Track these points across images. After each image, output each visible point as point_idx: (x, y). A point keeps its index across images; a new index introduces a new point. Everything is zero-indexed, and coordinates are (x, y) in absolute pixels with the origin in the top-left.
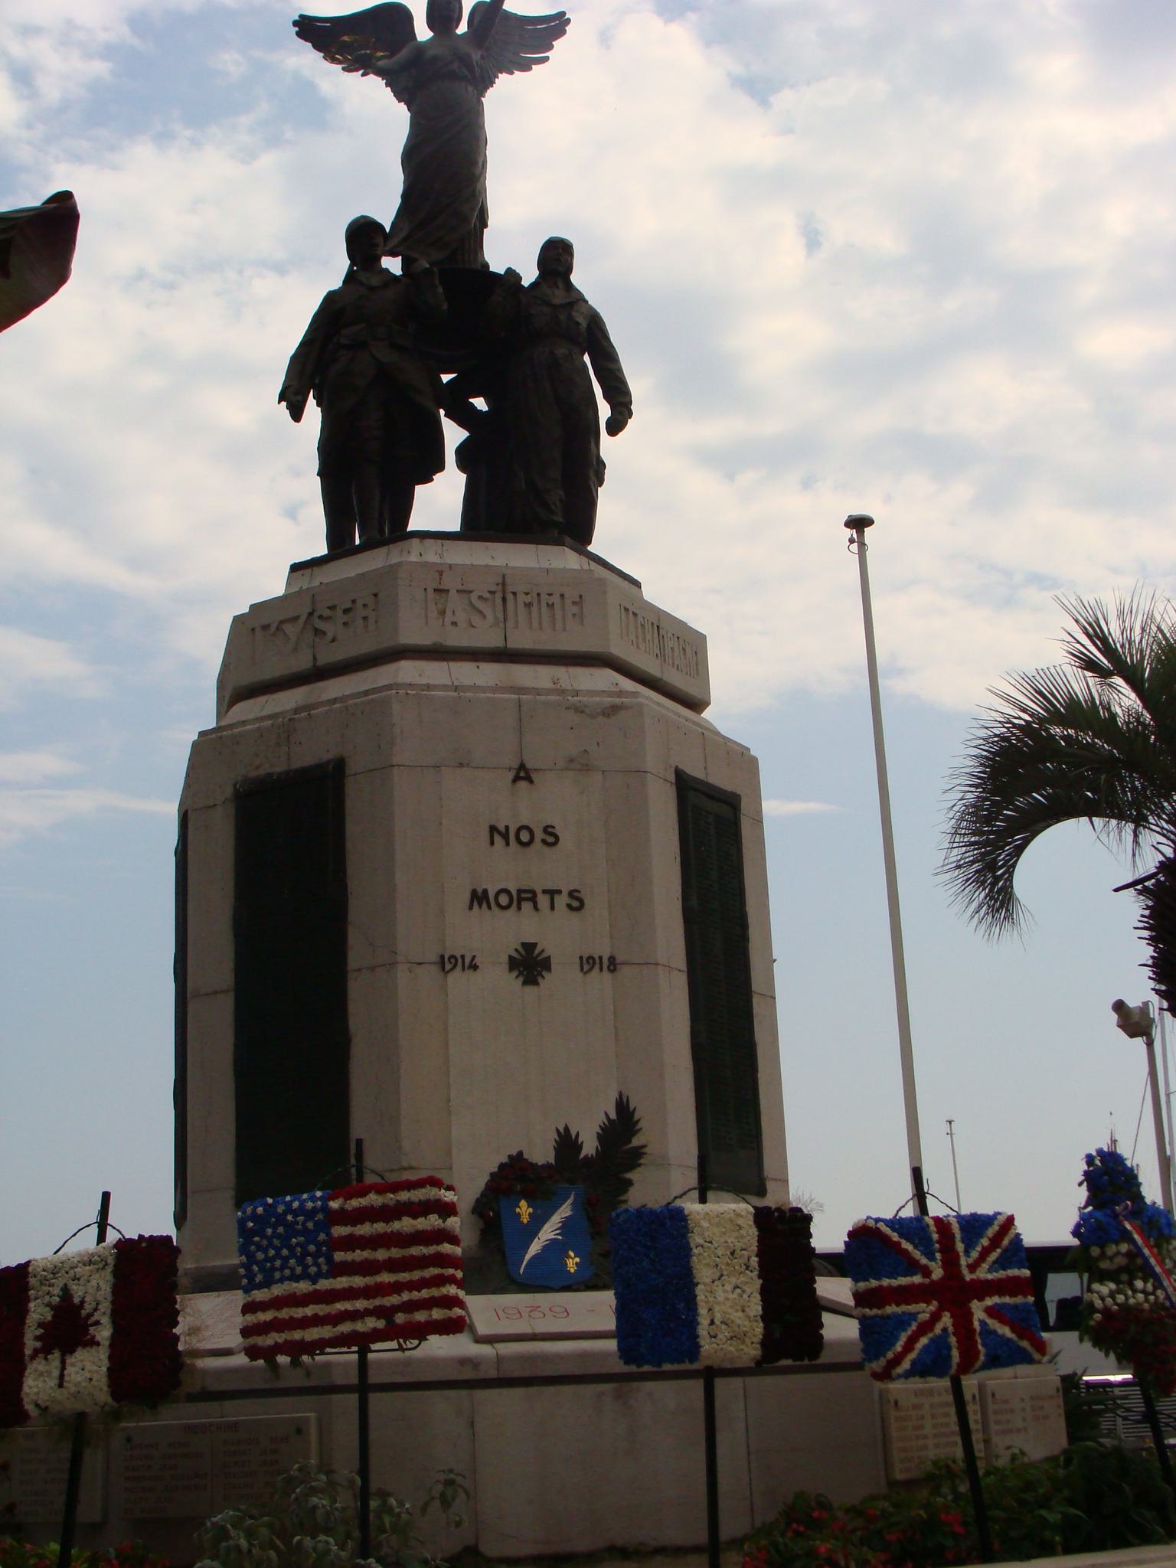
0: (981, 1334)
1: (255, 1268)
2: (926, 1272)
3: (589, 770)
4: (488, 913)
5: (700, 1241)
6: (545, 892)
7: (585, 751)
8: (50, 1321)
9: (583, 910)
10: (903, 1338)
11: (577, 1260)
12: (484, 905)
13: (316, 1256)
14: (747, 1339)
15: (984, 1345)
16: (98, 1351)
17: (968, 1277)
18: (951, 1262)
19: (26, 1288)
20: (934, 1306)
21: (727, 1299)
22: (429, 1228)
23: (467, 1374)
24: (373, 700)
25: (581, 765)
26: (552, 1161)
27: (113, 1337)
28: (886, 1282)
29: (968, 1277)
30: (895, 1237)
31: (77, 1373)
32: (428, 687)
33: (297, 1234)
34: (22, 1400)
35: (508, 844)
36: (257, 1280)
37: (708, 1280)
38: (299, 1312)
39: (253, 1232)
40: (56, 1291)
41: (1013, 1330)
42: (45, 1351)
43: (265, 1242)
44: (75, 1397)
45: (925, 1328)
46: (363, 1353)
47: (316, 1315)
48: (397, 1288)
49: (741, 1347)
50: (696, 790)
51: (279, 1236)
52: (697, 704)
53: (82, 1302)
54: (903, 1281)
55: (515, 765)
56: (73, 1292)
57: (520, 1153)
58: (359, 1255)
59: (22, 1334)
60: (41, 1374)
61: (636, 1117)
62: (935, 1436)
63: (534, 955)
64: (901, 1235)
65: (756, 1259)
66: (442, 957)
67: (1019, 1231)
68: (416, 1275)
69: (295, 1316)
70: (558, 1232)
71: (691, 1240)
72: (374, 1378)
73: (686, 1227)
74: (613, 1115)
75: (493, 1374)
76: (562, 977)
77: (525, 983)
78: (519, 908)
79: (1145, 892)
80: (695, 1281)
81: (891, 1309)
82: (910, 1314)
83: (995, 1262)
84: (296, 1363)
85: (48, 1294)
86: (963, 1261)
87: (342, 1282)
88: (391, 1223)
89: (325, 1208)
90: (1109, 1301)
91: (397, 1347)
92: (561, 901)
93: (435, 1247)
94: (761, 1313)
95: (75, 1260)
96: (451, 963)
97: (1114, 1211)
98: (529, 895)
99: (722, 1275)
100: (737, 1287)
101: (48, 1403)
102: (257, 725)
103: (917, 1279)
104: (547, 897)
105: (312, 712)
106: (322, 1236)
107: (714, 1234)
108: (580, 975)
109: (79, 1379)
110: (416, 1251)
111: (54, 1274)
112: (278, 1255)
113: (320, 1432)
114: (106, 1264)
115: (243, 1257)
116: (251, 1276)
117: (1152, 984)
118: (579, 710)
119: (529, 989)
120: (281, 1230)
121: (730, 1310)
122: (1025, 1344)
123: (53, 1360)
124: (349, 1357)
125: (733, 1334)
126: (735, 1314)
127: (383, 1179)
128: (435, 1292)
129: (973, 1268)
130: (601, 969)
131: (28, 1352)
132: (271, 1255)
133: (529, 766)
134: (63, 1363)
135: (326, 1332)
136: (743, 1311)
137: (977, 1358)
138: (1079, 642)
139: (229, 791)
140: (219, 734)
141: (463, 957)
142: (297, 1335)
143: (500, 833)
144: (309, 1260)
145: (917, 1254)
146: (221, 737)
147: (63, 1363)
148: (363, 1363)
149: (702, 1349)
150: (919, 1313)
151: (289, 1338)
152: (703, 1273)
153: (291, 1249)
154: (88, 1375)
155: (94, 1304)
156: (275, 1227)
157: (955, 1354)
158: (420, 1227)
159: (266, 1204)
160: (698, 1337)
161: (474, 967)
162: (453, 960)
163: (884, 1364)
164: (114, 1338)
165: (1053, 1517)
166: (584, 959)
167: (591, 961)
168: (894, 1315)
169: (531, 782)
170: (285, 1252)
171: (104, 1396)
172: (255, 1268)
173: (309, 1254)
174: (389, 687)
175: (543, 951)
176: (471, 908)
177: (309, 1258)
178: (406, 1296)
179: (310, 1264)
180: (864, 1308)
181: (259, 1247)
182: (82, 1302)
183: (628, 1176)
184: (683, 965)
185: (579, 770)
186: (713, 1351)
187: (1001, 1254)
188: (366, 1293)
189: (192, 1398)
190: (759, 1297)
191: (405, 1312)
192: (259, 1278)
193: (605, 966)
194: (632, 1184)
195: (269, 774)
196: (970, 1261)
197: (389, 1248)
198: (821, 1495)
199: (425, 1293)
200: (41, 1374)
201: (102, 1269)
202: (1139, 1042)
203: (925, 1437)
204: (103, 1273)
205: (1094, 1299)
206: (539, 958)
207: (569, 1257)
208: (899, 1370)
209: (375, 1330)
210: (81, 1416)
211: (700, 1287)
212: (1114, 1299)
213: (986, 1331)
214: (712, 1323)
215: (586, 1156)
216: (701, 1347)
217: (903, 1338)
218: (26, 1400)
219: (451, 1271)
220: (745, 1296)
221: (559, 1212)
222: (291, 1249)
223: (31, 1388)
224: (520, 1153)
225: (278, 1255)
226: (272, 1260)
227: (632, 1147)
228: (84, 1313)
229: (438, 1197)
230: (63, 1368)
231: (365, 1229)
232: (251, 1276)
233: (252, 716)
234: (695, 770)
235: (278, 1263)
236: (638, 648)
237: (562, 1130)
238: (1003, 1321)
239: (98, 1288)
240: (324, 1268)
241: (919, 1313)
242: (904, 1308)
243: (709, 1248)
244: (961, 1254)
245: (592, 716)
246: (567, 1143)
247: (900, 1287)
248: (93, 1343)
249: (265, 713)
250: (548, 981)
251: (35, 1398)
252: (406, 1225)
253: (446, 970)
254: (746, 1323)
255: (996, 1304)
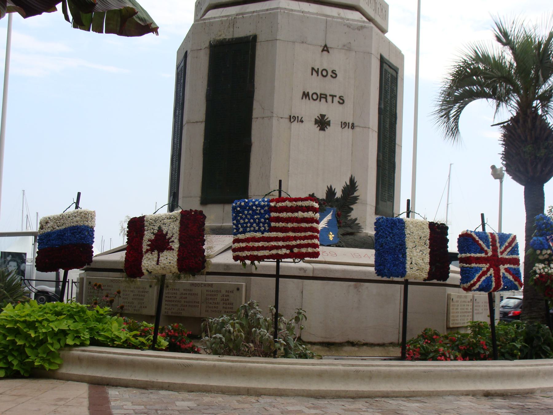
0: (502, 278)
1: (240, 226)
2: (486, 253)
3: (350, 50)
4: (309, 101)
5: (409, 232)
6: (330, 95)
7: (350, 43)
8: (153, 240)
9: (344, 104)
10: (477, 276)
11: (333, 236)
12: (307, 98)
13: (264, 223)
14: (423, 271)
15: (503, 282)
16: (173, 252)
17: (500, 256)
18: (495, 250)
19: (143, 226)
20: (488, 265)
21: (417, 255)
22: (309, 217)
23: (302, 274)
24: (270, 13)
25: (347, 48)
26: (325, 198)
27: (179, 248)
28: (473, 255)
29: (500, 256)
30: (477, 238)
31: (164, 260)
32: (292, 10)
33: (257, 214)
34: (142, 268)
35: (318, 75)
36: (240, 231)
37: (411, 247)
38: (256, 244)
39: (239, 212)
40: (156, 228)
41: (513, 278)
42: (151, 250)
43: (244, 216)
44: (163, 269)
45: (484, 273)
46: (278, 263)
47: (263, 246)
48: (295, 238)
49: (421, 273)
50: (386, 63)
51: (250, 214)
52: (384, 31)
53: (167, 233)
54: (478, 255)
55: (323, 45)
56: (163, 229)
57: (313, 194)
58: (281, 225)
59: (141, 243)
60: (149, 259)
61: (356, 185)
62: (461, 313)
63: (325, 119)
64: (479, 238)
65: (429, 241)
66: (290, 116)
67: (517, 241)
68: (303, 234)
69: (255, 246)
70: (326, 224)
71: (406, 231)
72: (281, 273)
73: (404, 226)
74: (348, 184)
75: (311, 275)
76: (334, 129)
77: (320, 130)
78: (320, 101)
79: (504, 127)
80: (406, 247)
81: (473, 265)
82: (480, 268)
83: (509, 252)
84: (252, 263)
85: (152, 229)
86: (499, 250)
87: (274, 234)
88: (294, 213)
89: (268, 205)
90: (542, 270)
91: (293, 261)
92: (336, 99)
93: (311, 224)
94: (429, 261)
95: (164, 217)
96: (293, 119)
97: (546, 238)
98: (324, 96)
99: (416, 246)
100: (421, 251)
101: (152, 270)
102: (221, 19)
103: (483, 255)
104: (331, 98)
105: (244, 16)
106: (267, 216)
107: (414, 230)
108: (341, 129)
109: (165, 262)
110: (304, 225)
111: (155, 221)
112: (249, 222)
113: (246, 290)
114: (177, 219)
115: (235, 221)
116: (238, 229)
117: (501, 161)
118: (349, 26)
119: (322, 132)
120: (251, 212)
121: (418, 259)
122: (516, 283)
123: (155, 254)
124: (272, 263)
125: (418, 268)
126: (420, 261)
127: (289, 196)
128: (310, 241)
129: (502, 253)
130: (349, 128)
131: (144, 250)
132: (246, 221)
133: (328, 46)
134: (159, 255)
135: (266, 253)
136: (423, 260)
137: (500, 286)
138: (495, 31)
139: (207, 44)
140: (204, 21)
141: (298, 117)
142: (255, 253)
143: (315, 71)
144: (261, 225)
145: (484, 246)
146: (205, 23)
147: (159, 255)
148: (278, 266)
149: (407, 273)
150: (482, 268)
151: (252, 254)
152: (409, 244)
153: (255, 220)
154: (169, 261)
155: (171, 235)
156: (248, 211)
157: (494, 284)
158: (305, 216)
159: (245, 202)
160: (406, 268)
161: (302, 121)
162: (294, 118)
163: (469, 285)
164: (180, 248)
165: (519, 346)
166: (343, 123)
167: (345, 124)
168: (475, 267)
169: (328, 52)
170: (252, 221)
171: (175, 269)
172: (240, 226)
173: (261, 222)
174: (277, 8)
175: (328, 118)
176: (302, 98)
177: (261, 224)
178: (298, 242)
179: (261, 226)
180: (463, 264)
181: (241, 218)
182: (167, 233)
183: (352, 206)
184: (377, 130)
185: (347, 50)
186: (411, 274)
187: (511, 249)
188: (284, 239)
189: (209, 273)
190: (429, 256)
191: (298, 248)
192: (241, 230)
193: (350, 127)
194: (353, 210)
195: (225, 39)
196: (501, 250)
197: (293, 223)
198: (436, 330)
199: (306, 242)
200: (149, 259)
201: (175, 221)
202: (498, 181)
203: (458, 312)
204: (175, 223)
205: (536, 269)
206: (326, 121)
207: (330, 234)
208: (474, 288)
209: (286, 254)
210: (164, 276)
211: (408, 249)
212: (544, 270)
213: (505, 277)
214: (411, 263)
215: (337, 197)
216: (407, 272)
217: (477, 276)
218: (143, 268)
219: (316, 234)
220: (424, 255)
221: (326, 217)
222: (255, 220)
223: (145, 264)
224: (313, 194)
225: (249, 222)
226: (247, 223)
227: (354, 196)
228: (167, 237)
229: (312, 205)
230: (159, 258)
231: (284, 215)
232: (238, 229)
233: (217, 16)
234: (386, 56)
235: (249, 225)
236: (368, 5)
237: (329, 187)
238: (510, 274)
239: (173, 229)
240: (267, 228)
241: (482, 268)
242: (478, 265)
243: (412, 235)
244: (499, 248)
245: (354, 29)
246: (331, 192)
247: (477, 257)
248: (171, 249)
249: (223, 14)
250: (329, 130)
251: (147, 268)
252: (300, 214)
253: (291, 121)
254: (424, 264)
255: (508, 267)
